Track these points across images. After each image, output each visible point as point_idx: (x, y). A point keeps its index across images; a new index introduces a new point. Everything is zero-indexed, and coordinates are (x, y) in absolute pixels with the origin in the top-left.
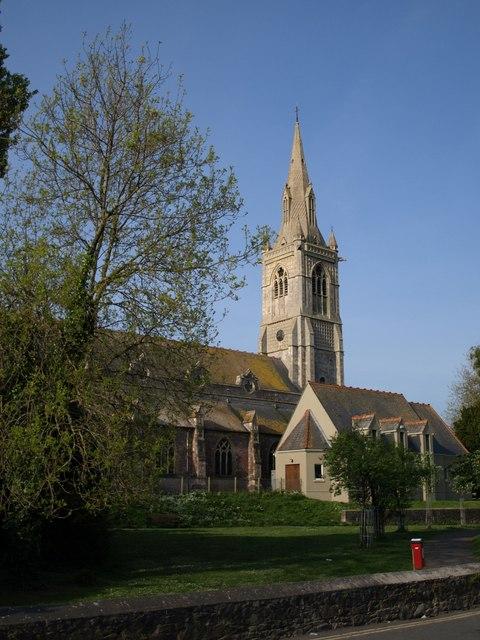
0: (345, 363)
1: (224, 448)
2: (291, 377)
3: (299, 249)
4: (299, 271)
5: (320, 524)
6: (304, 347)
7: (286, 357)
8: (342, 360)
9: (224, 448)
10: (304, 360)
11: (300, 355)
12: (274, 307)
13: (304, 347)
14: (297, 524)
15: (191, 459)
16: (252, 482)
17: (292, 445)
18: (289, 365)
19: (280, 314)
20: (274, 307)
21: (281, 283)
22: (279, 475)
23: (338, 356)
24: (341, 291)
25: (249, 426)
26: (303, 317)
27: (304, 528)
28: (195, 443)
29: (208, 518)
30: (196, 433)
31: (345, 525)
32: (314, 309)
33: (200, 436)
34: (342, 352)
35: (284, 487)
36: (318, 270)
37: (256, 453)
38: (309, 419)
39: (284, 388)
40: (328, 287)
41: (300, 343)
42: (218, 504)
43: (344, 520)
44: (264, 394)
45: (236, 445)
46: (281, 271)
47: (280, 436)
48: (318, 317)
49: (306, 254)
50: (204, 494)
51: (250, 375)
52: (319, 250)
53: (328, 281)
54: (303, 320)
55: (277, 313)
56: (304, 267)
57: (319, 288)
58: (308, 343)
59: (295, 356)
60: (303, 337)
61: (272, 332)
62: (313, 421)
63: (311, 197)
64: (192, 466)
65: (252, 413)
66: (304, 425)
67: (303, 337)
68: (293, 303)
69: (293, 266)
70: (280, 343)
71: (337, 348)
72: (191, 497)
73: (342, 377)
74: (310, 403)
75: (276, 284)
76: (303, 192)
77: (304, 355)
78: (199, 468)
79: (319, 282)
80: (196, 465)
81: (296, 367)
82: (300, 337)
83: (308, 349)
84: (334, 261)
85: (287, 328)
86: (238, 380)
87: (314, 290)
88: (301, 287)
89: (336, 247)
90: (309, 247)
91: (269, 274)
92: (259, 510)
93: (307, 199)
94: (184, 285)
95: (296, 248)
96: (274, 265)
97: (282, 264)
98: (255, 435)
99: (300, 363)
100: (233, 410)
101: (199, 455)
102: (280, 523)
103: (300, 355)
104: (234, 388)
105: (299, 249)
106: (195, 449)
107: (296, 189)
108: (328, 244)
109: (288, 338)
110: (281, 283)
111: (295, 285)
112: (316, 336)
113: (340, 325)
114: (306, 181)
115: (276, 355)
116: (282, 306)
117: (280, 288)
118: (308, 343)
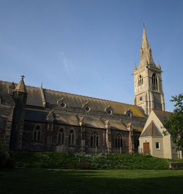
0: (165, 108)
1: (119, 137)
2: (145, 113)
3: (147, 67)
4: (147, 75)
5: (159, 169)
6: (150, 102)
7: (143, 106)
8: (164, 107)
9: (119, 137)
10: (150, 107)
11: (148, 105)
12: (138, 89)
13: (150, 102)
14: (148, 169)
15: (105, 141)
16: (131, 151)
17: (146, 135)
18: (144, 108)
19: (141, 91)
20: (138, 89)
21: (141, 81)
22: (141, 147)
23: (163, 105)
24: (163, 83)
25: (129, 129)
26: (149, 91)
27: (152, 171)
28: (107, 135)
29: (106, 165)
30: (107, 131)
31: (171, 169)
32: (153, 89)
33: (109, 132)
34: (164, 104)
35: (143, 152)
36: (154, 75)
37: (132, 139)
38: (153, 124)
39: (143, 116)
40: (158, 81)
41: (148, 100)
42: (112, 159)
43: (170, 167)
44: (135, 118)
45: (124, 136)
46: (140, 76)
47: (141, 133)
48: (155, 91)
49: (149, 69)
50: (106, 154)
51: (129, 111)
52: (154, 68)
53: (158, 79)
54: (149, 92)
55: (140, 91)
56: (149, 74)
57: (155, 81)
58: (151, 100)
59: (147, 105)
60: (149, 98)
61: (138, 98)
62: (155, 125)
63: (150, 51)
64: (106, 143)
65: (130, 124)
66: (151, 127)
67: (149, 98)
68: (145, 86)
69: (145, 74)
70: (141, 101)
71: (162, 103)
72: (100, 155)
73: (164, 108)
74: (153, 118)
75: (139, 81)
76: (147, 49)
77: (150, 105)
78: (109, 145)
79: (154, 79)
80: (107, 143)
81: (147, 109)
82: (148, 98)
83: (152, 102)
84: (160, 72)
85: (143, 96)
86: (125, 113)
87: (153, 82)
88: (148, 81)
89: (160, 67)
90: (150, 67)
91: (136, 78)
92: (131, 162)
93: (149, 51)
94: (146, 162)
95: (145, 67)
96: (138, 74)
97: (141, 74)
98: (131, 132)
99: (148, 108)
100: (123, 124)
101: (109, 139)
102: (140, 168)
103: (148, 105)
104: (123, 115)
105: (147, 67)
106: (107, 137)
107: (145, 49)
108: (157, 66)
109: (144, 99)
110: (141, 81)
111: (146, 80)
112: (154, 98)
113: (163, 94)
114: (148, 46)
115: (140, 106)
116: (141, 88)
117: (141, 82)
118: (151, 100)
